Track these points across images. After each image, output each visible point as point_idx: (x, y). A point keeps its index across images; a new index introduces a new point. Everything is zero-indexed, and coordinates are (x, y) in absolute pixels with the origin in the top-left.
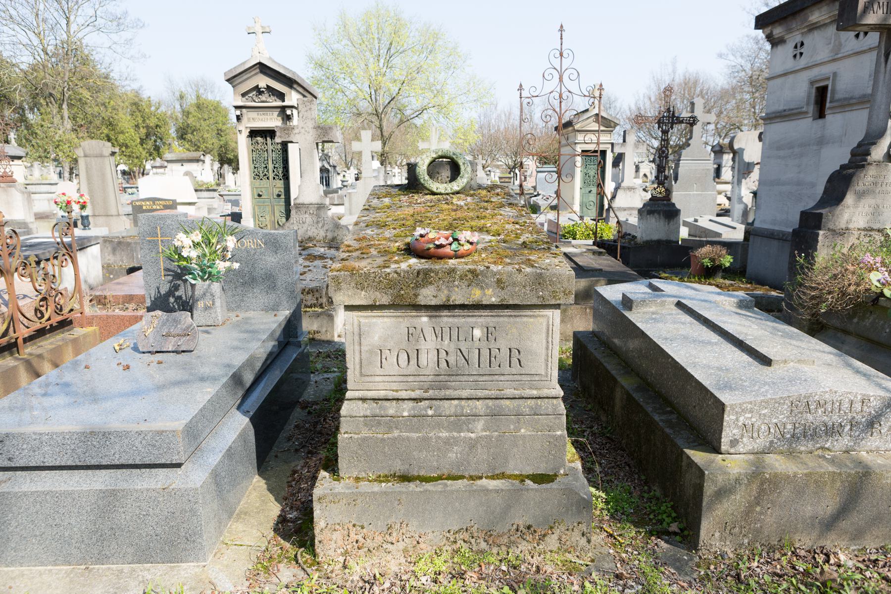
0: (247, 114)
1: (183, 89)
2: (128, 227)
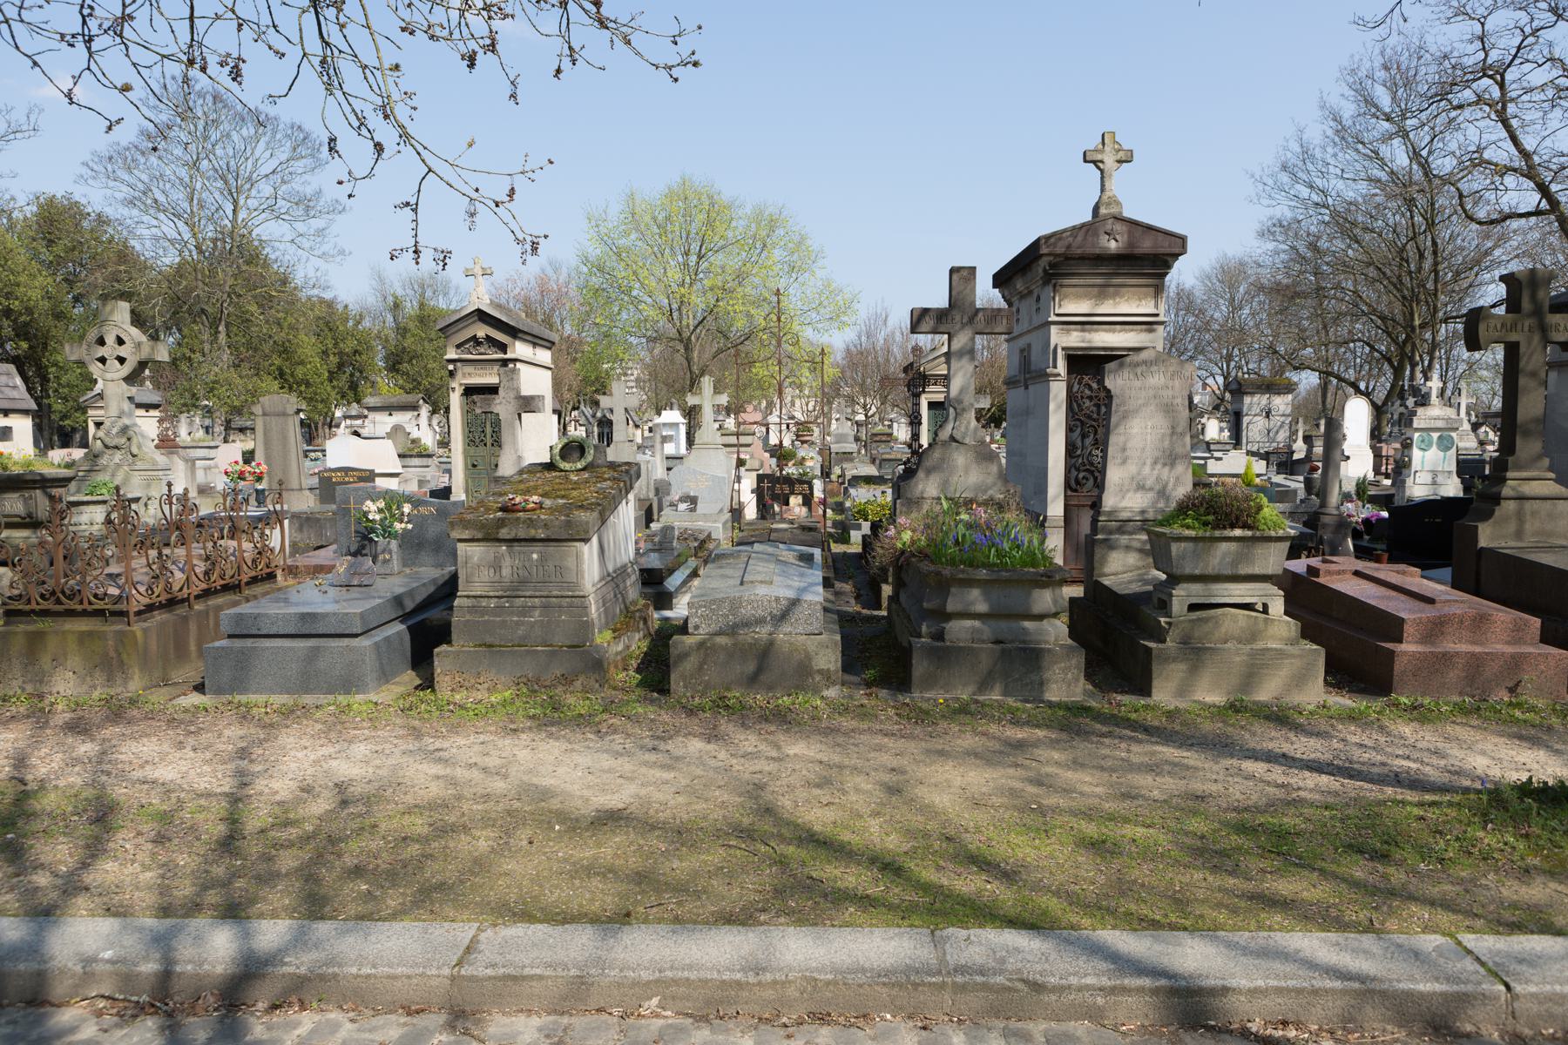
0: (463, 369)
1: (400, 292)
2: (312, 504)
